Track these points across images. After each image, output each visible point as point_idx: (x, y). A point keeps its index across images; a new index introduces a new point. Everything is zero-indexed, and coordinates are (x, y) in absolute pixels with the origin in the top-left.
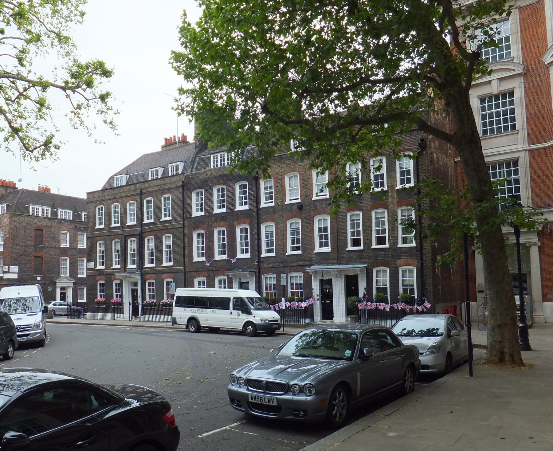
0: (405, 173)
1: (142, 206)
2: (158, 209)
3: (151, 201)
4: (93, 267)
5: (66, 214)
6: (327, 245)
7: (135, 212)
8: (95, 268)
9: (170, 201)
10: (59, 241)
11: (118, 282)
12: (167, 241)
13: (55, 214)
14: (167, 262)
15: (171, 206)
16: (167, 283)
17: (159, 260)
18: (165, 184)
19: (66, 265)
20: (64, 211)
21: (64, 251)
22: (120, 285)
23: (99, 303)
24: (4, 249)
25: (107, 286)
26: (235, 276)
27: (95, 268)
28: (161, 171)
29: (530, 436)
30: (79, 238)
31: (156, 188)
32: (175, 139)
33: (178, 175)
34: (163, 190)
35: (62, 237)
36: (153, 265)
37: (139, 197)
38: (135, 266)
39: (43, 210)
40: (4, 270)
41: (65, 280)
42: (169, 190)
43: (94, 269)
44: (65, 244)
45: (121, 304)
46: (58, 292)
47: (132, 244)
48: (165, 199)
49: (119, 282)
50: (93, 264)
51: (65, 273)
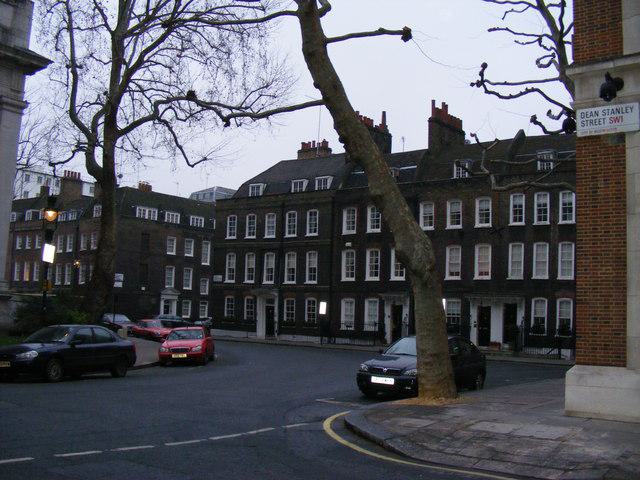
0: (567, 209)
1: (284, 219)
3: (294, 215)
5: (172, 217)
6: (521, 220)
10: (165, 249)
11: (251, 298)
12: (312, 261)
13: (161, 216)
17: (301, 278)
18: (312, 199)
19: (171, 275)
20: (143, 209)
22: (254, 301)
23: (226, 320)
25: (239, 301)
26: (388, 299)
28: (305, 183)
31: (301, 202)
32: (314, 145)
33: (325, 190)
34: (309, 204)
35: (168, 244)
38: (272, 282)
39: (150, 211)
41: (170, 292)
42: (316, 206)
45: (255, 322)
46: (162, 304)
47: (270, 262)
50: (220, 277)
51: (170, 285)
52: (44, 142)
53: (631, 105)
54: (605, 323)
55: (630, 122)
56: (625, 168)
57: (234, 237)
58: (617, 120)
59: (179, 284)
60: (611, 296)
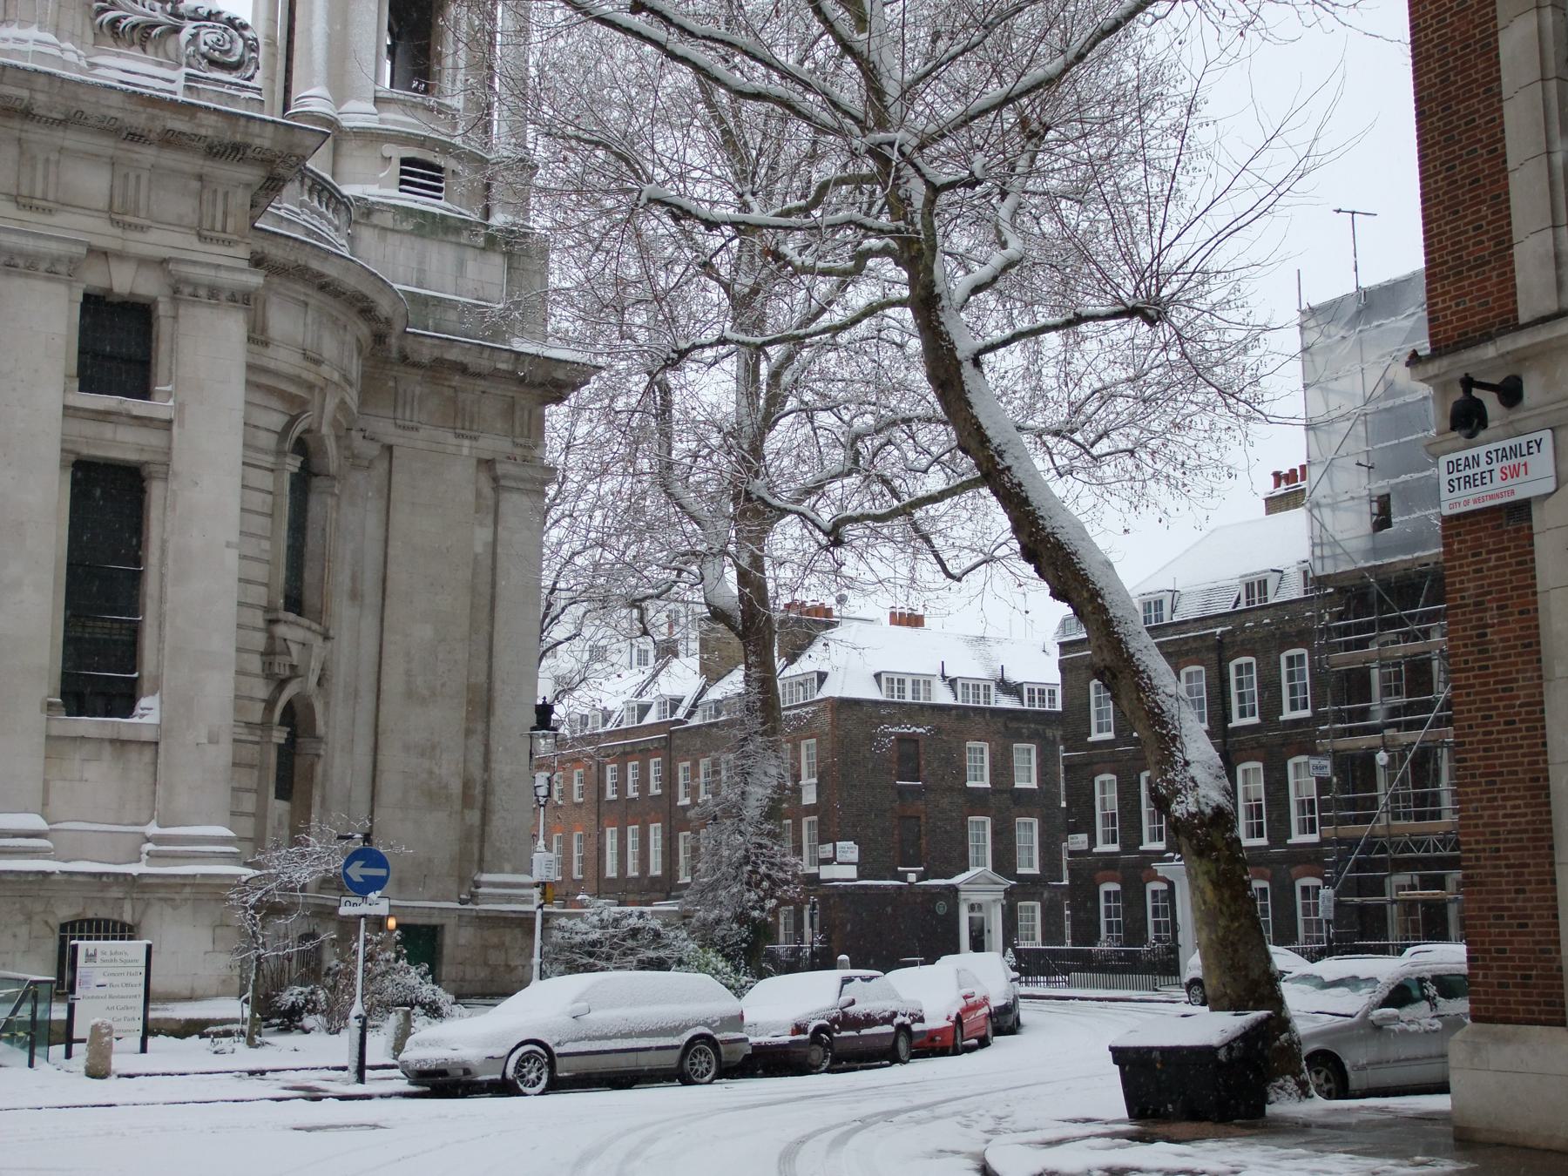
2: (1270, 687)
4: (1085, 847)
7: (1205, 696)
8: (1090, 849)
9: (1307, 667)
11: (1162, 887)
14: (1303, 831)
15: (1308, 680)
16: (1305, 889)
17: (1280, 829)
19: (981, 830)
21: (978, 801)
24: (818, 795)
27: (1090, 849)
29: (903, 606)
30: (1018, 761)
36: (1263, 841)
37: (1213, 656)
40: (822, 856)
43: (1089, 852)
44: (980, 780)
48: (1290, 660)
49: (1164, 887)
52: (688, 461)
53: (1536, 436)
54: (1521, 926)
55: (1536, 477)
56: (1534, 577)
57: (1255, 720)
58: (1515, 472)
59: (1004, 862)
60: (1528, 865)
